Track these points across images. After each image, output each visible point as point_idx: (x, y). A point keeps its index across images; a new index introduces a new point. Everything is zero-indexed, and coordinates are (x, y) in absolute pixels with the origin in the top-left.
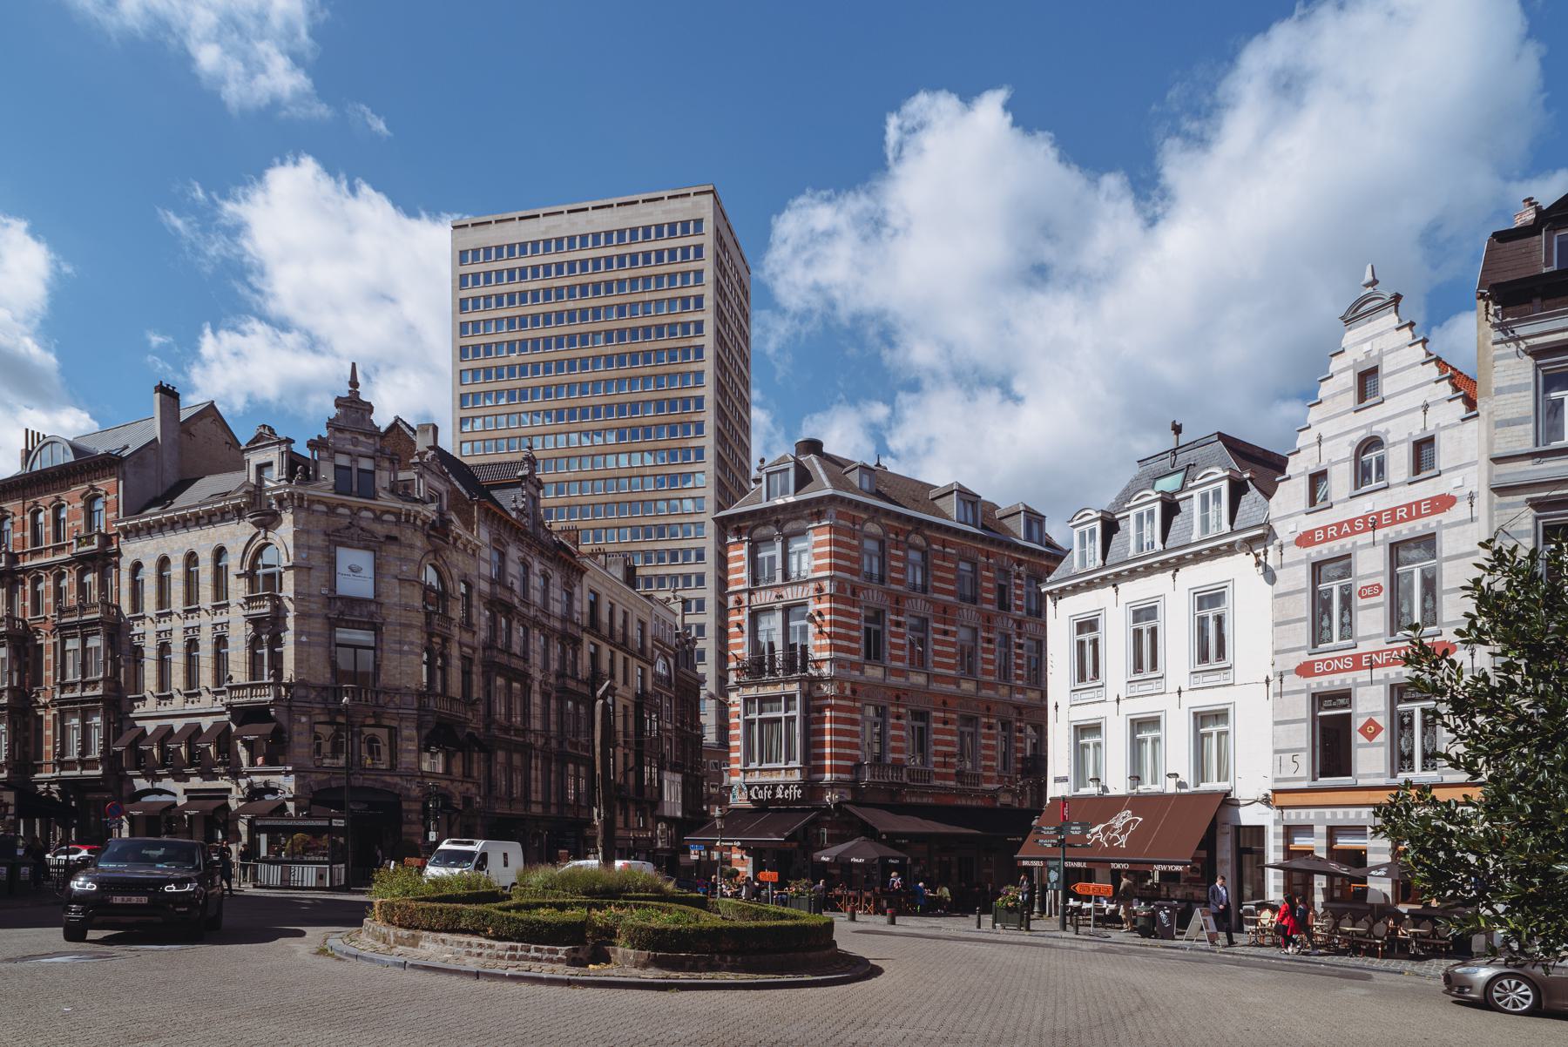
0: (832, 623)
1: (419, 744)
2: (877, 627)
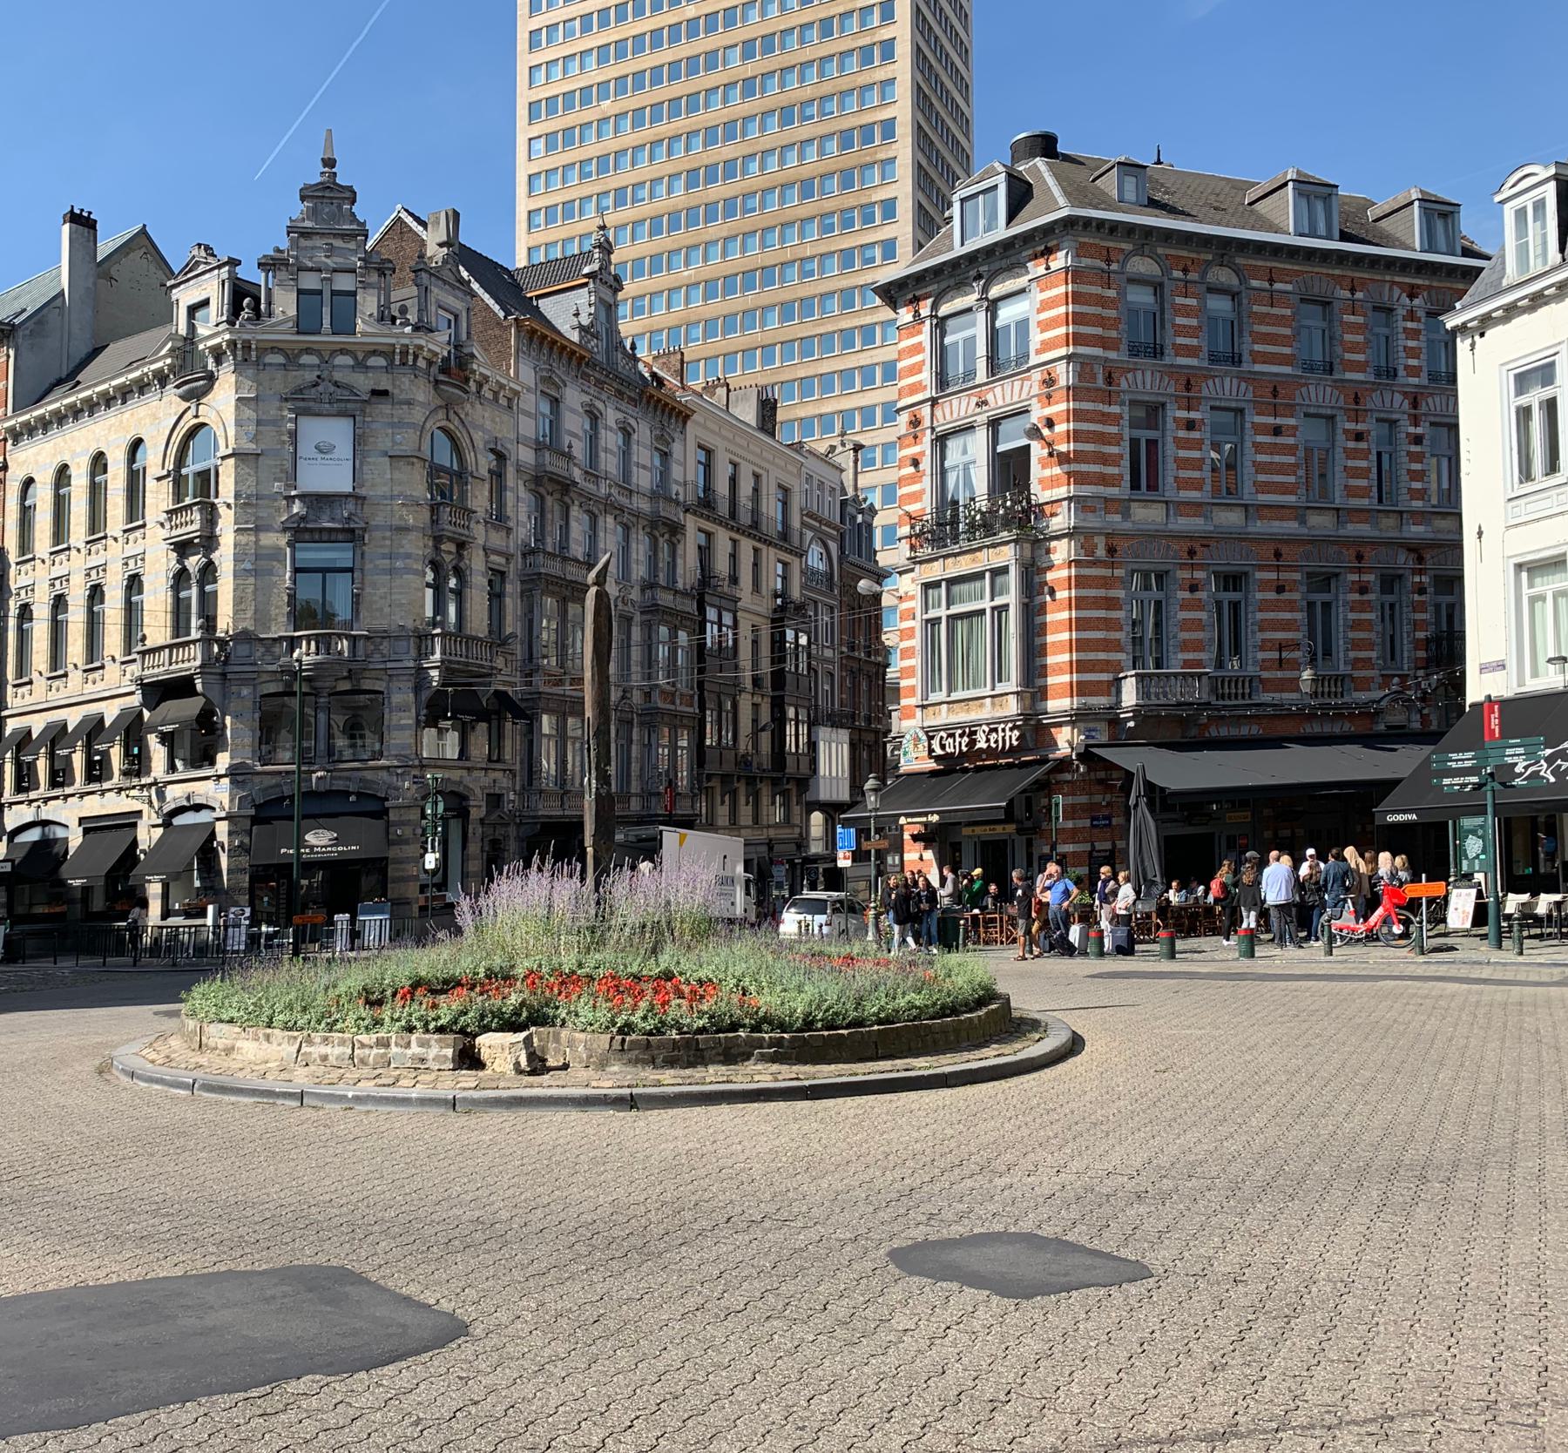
0: (1077, 436)
1: (418, 715)
2: (1152, 434)
